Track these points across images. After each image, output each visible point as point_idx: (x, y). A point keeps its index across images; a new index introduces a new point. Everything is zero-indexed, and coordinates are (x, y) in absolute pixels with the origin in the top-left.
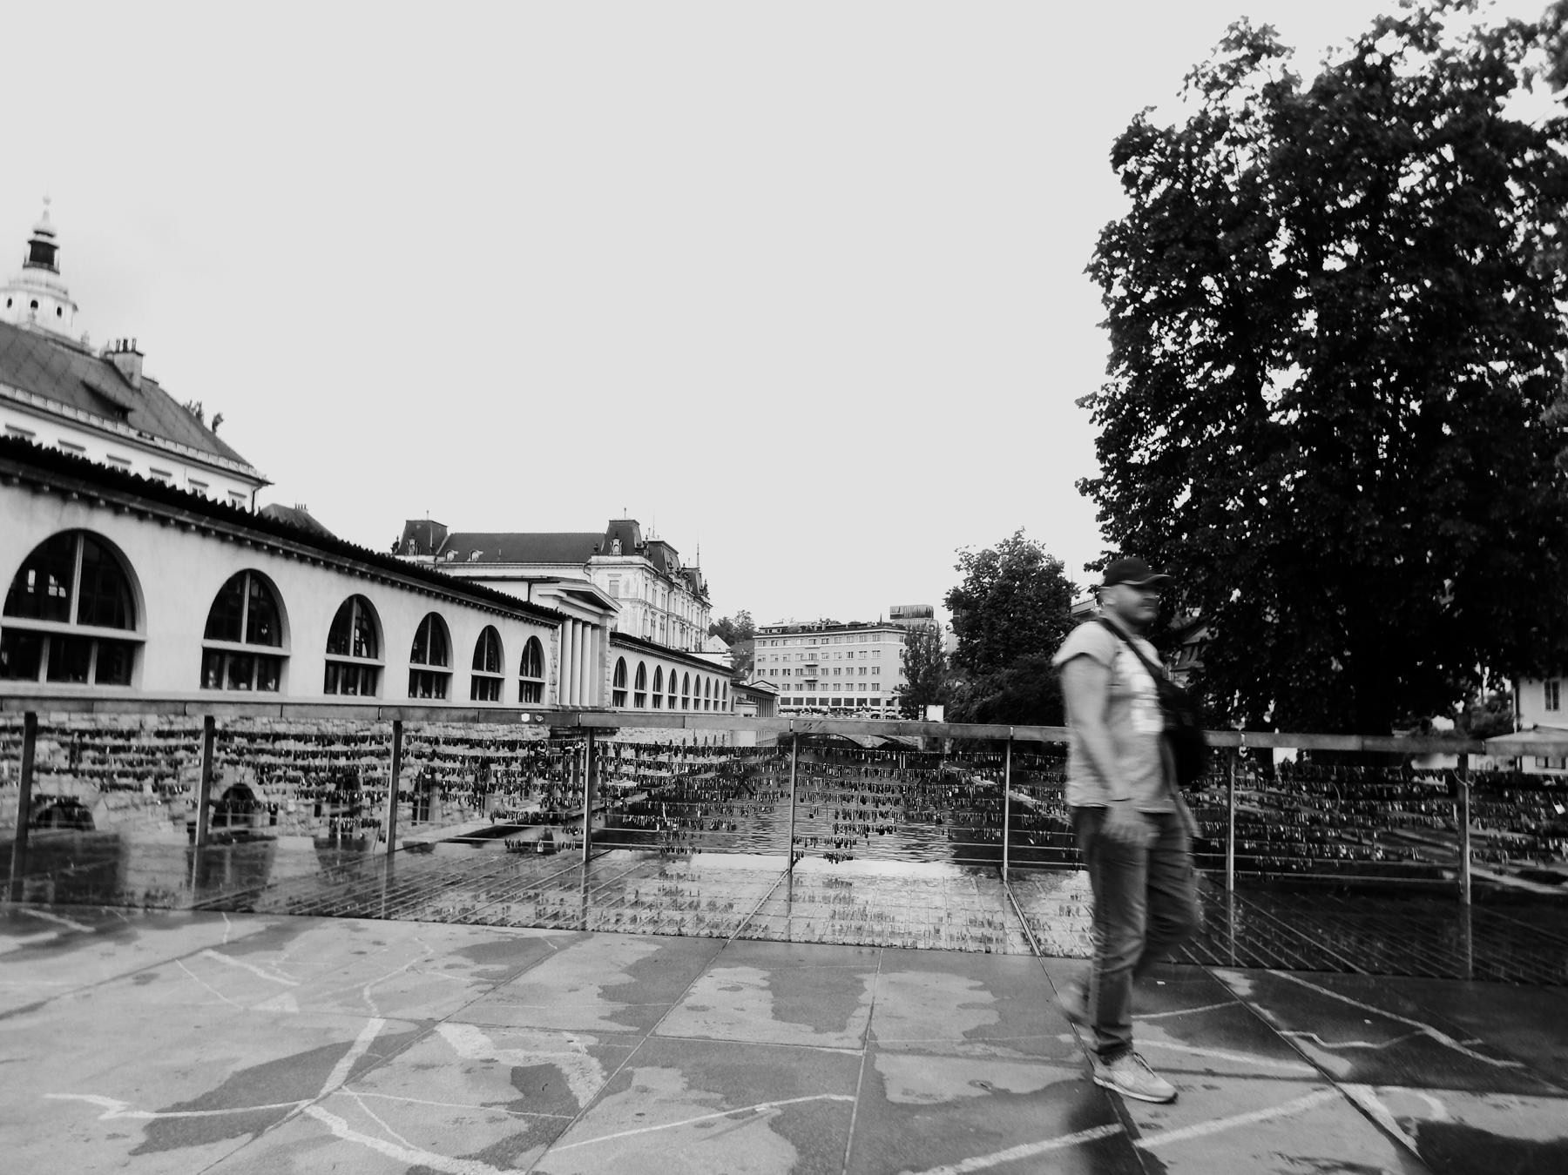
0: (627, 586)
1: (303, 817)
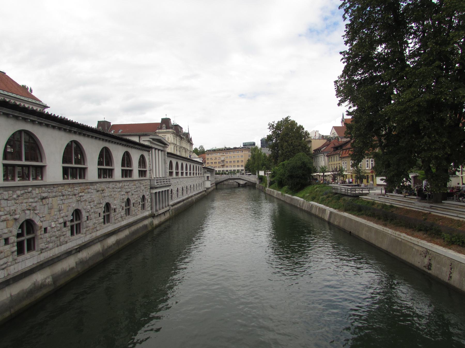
1: (59, 229)
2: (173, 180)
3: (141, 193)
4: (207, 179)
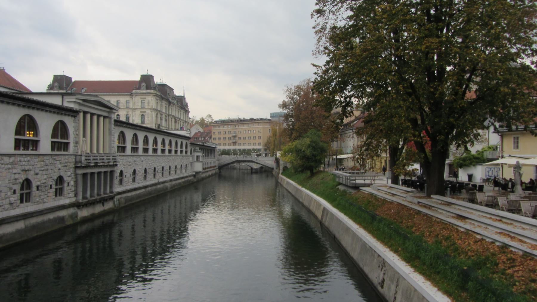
0: (149, 103)
2: (120, 157)
3: (55, 172)
4: (197, 160)
